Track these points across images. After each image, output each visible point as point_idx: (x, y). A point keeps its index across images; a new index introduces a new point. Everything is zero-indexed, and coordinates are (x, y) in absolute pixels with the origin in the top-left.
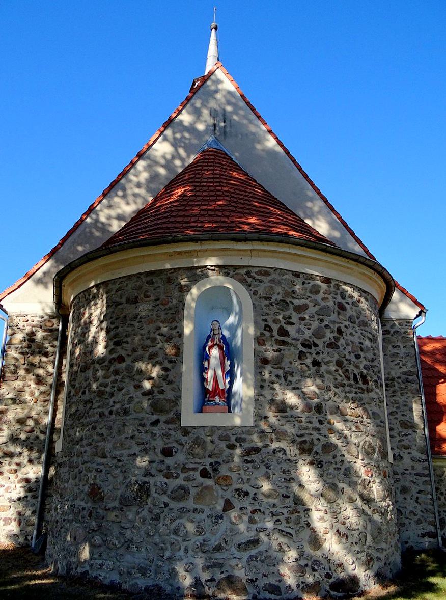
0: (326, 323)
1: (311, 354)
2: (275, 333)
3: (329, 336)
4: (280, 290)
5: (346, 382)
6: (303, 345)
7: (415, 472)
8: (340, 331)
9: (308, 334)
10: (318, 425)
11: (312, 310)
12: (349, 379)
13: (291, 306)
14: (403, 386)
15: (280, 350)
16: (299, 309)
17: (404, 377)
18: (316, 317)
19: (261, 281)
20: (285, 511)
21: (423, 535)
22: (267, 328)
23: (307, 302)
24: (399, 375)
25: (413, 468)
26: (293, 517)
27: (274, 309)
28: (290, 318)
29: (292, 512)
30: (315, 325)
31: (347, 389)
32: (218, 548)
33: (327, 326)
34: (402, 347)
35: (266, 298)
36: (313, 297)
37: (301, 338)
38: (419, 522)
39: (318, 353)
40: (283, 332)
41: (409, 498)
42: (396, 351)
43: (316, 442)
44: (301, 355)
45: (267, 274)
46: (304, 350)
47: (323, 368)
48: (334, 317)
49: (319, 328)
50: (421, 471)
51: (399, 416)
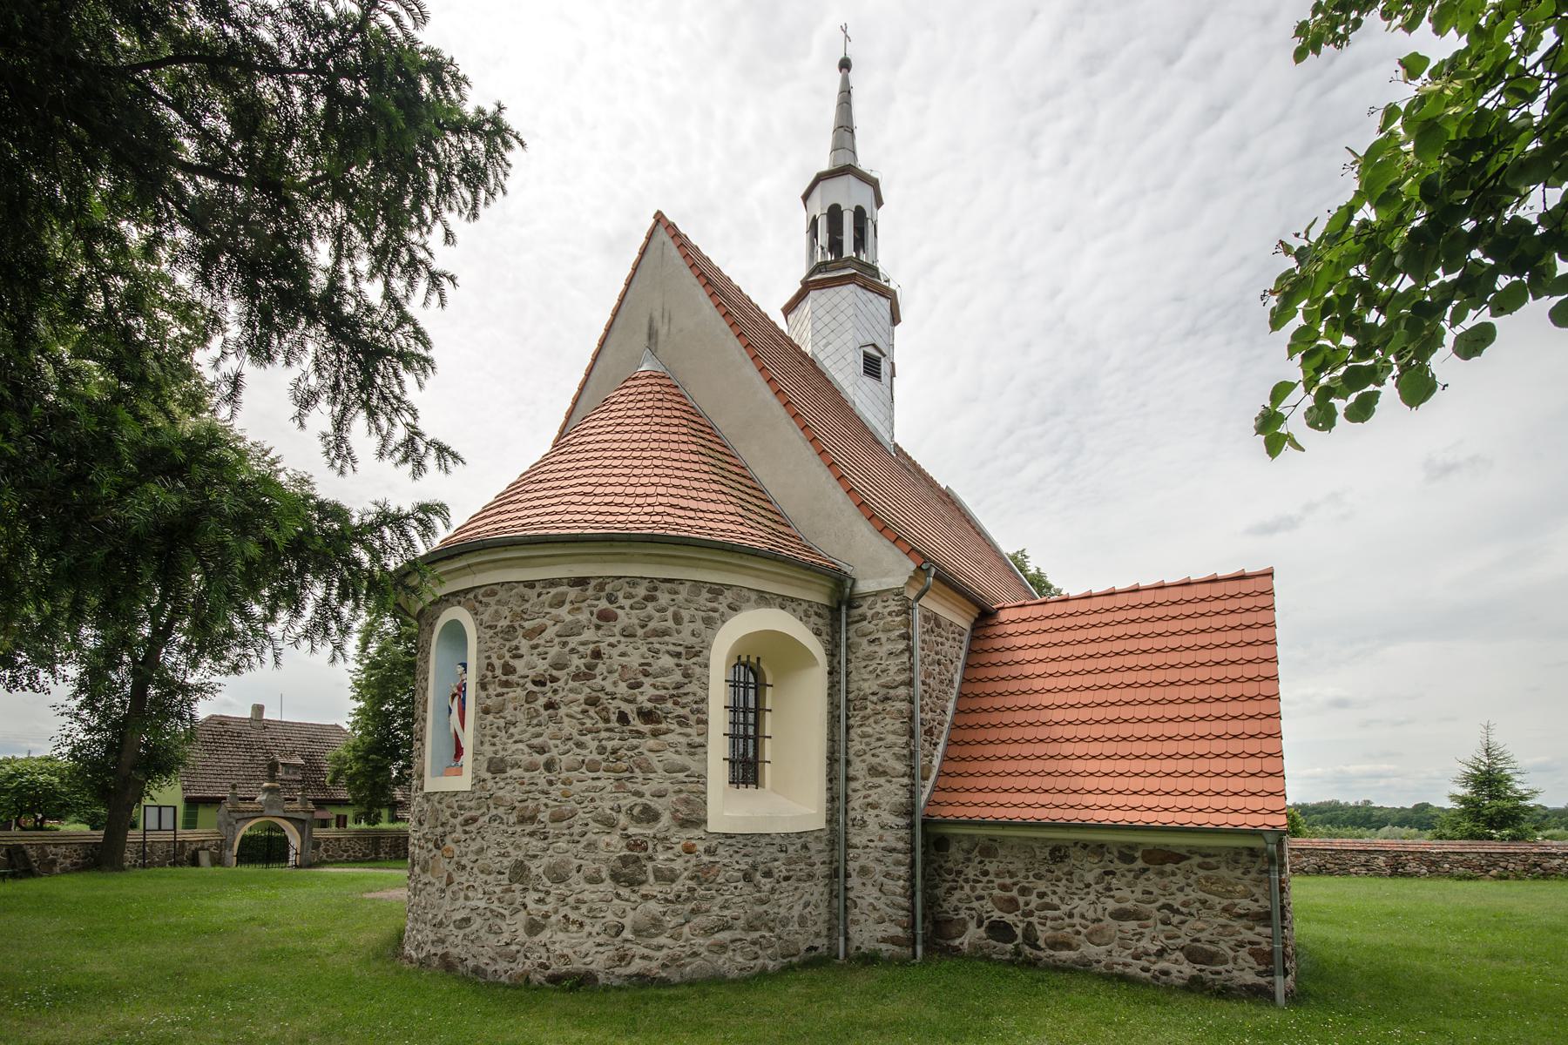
0: (571, 645)
1: (544, 694)
2: (498, 672)
3: (576, 662)
4: (507, 613)
5: (601, 725)
6: (535, 683)
7: (883, 844)
8: (597, 654)
9: (542, 666)
10: (546, 787)
11: (551, 632)
12: (607, 721)
13: (520, 632)
14: (879, 707)
15: (502, 695)
16: (529, 634)
17: (883, 692)
18: (557, 640)
19: (487, 605)
20: (498, 889)
21: (884, 940)
22: (490, 667)
23: (544, 621)
24: (875, 688)
25: (881, 839)
26: (508, 896)
27: (499, 641)
28: (517, 648)
29: (505, 891)
30: (554, 651)
31: (604, 734)
32: (441, 924)
33: (573, 651)
34: (884, 640)
35: (490, 627)
36: (554, 611)
37: (532, 673)
38: (881, 921)
39: (555, 692)
40: (508, 669)
41: (869, 883)
42: (873, 648)
43: (543, 808)
44: (530, 697)
45: (494, 593)
46: (536, 689)
47: (563, 711)
48: (588, 635)
49: (559, 655)
50: (894, 844)
51: (868, 757)
